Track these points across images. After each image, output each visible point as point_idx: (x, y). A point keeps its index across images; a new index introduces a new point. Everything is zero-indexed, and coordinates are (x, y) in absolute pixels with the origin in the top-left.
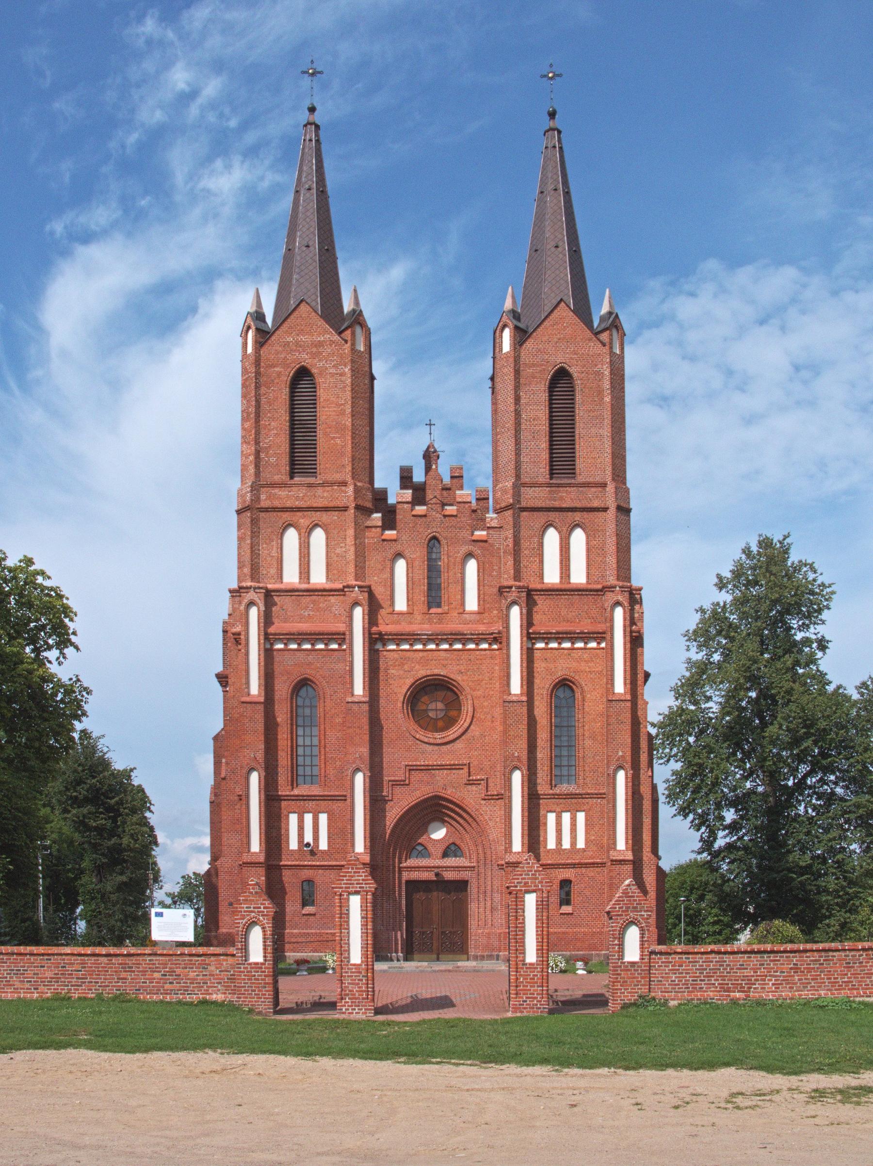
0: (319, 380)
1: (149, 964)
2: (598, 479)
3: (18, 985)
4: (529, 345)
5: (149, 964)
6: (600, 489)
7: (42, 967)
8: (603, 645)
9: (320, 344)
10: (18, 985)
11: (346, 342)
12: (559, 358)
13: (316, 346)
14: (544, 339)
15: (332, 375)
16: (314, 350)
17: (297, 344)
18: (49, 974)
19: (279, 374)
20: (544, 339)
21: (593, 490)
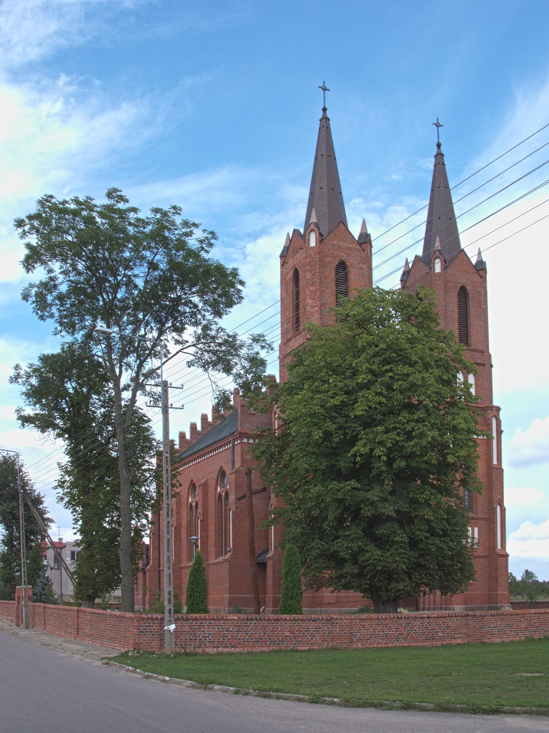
0: (350, 269)
1: (272, 631)
2: (480, 348)
3: (509, 633)
4: (449, 271)
5: (272, 631)
6: (481, 354)
7: (521, 621)
8: (485, 437)
9: (350, 249)
10: (509, 633)
11: (364, 251)
12: (463, 281)
13: (348, 249)
14: (456, 269)
15: (357, 268)
16: (348, 252)
17: (339, 245)
18: (523, 626)
19: (330, 262)
20: (456, 269)
21: (478, 354)
